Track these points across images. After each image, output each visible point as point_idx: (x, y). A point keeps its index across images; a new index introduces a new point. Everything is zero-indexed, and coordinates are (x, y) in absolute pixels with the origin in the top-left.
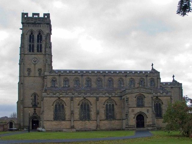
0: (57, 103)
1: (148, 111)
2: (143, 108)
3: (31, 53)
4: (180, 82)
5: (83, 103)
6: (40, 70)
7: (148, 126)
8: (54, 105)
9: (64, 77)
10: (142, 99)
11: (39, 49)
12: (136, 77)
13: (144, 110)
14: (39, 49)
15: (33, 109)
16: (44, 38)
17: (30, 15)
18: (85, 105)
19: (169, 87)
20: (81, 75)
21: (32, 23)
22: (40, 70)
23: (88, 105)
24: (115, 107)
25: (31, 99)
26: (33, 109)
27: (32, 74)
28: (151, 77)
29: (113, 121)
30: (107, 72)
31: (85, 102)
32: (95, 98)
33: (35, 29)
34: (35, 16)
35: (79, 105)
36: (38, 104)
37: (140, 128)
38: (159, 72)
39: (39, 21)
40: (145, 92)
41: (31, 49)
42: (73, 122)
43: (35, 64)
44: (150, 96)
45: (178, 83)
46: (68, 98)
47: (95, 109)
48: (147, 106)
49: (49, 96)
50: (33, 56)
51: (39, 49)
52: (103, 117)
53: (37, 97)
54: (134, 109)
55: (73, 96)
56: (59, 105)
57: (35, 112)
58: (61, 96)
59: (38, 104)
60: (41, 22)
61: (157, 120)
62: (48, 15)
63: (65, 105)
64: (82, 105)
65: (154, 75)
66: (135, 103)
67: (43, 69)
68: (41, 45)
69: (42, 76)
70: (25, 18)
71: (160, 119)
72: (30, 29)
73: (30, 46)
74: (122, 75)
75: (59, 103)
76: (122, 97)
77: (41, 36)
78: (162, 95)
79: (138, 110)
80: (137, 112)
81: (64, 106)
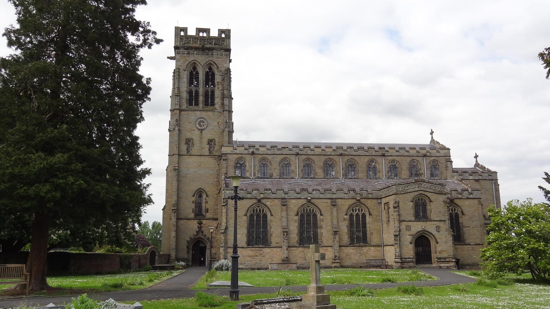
0: (254, 211)
1: (438, 229)
2: (429, 223)
3: (193, 107)
4: (493, 169)
5: (304, 211)
6: (211, 142)
7: (440, 260)
8: (248, 214)
9: (260, 156)
10: (424, 205)
11: (209, 100)
13: (430, 227)
15: (196, 222)
16: (218, 78)
17: (192, 32)
18: (308, 215)
19: (471, 178)
21: (196, 49)
22: (211, 142)
23: (315, 216)
24: (368, 219)
25: (193, 202)
26: (196, 222)
27: (195, 150)
28: (433, 158)
29: (365, 249)
30: (301, 147)
31: (258, 209)
33: (202, 60)
34: (201, 34)
35: (297, 215)
36: (208, 212)
37: (424, 264)
38: (449, 149)
39: (210, 44)
40: (431, 191)
41: (193, 99)
42: (287, 249)
43: (201, 130)
44: (441, 199)
45: (489, 171)
46: (276, 201)
47: (330, 224)
48: (436, 219)
50: (198, 114)
52: (346, 239)
53: (204, 196)
54: (410, 223)
56: (258, 216)
57: (200, 228)
58: (262, 196)
59: (208, 212)
60: (213, 46)
62: (227, 32)
63: (319, 215)
64: (302, 216)
66: (412, 212)
68: (213, 92)
69: (217, 154)
70: (181, 38)
71: (460, 246)
72: (193, 59)
73: (190, 93)
74: (374, 153)
75: (257, 210)
76: (381, 199)
77: (213, 74)
78: (460, 196)
79: (417, 227)
80: (416, 231)
81: (267, 218)
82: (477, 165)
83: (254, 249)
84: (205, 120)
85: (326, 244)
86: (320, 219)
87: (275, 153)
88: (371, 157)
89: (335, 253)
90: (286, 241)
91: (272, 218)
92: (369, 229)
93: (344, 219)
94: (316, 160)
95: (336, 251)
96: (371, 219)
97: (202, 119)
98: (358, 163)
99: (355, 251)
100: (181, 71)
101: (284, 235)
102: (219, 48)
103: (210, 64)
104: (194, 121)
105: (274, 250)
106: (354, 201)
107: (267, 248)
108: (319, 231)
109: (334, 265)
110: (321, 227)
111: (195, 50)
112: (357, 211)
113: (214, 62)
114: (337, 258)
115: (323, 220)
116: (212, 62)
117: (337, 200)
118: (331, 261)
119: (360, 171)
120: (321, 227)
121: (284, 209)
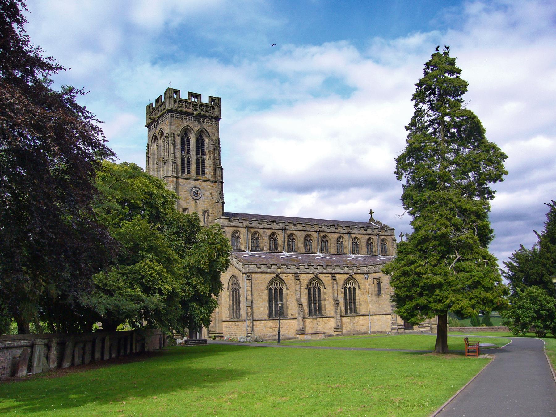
12: (362, 235)
14: (200, 168)
20: (347, 232)
32: (330, 276)
34: (193, 99)
42: (303, 321)
46: (290, 275)
47: (331, 296)
49: (259, 270)
51: (200, 168)
55: (298, 271)
61: (221, 332)
65: (386, 234)
67: (210, 210)
82: (372, 219)
83: (275, 321)
84: (199, 189)
85: (329, 315)
86: (324, 292)
87: (265, 227)
88: (340, 235)
89: (337, 322)
90: (301, 313)
91: (288, 291)
92: (358, 300)
93: (341, 292)
94: (298, 235)
95: (338, 321)
96: (360, 292)
97: (196, 189)
98: (330, 239)
99: (349, 320)
100: (176, 136)
101: (300, 307)
102: (210, 116)
103: (202, 131)
104: (189, 189)
105: (290, 321)
106: (348, 276)
107: (285, 320)
108: (323, 303)
109: (336, 333)
110: (325, 300)
111: (188, 115)
112: (350, 284)
113: (206, 130)
114: (339, 327)
115: (325, 293)
116: (204, 130)
117: (336, 275)
118: (333, 329)
119: (332, 247)
120: (325, 300)
121: (297, 283)
